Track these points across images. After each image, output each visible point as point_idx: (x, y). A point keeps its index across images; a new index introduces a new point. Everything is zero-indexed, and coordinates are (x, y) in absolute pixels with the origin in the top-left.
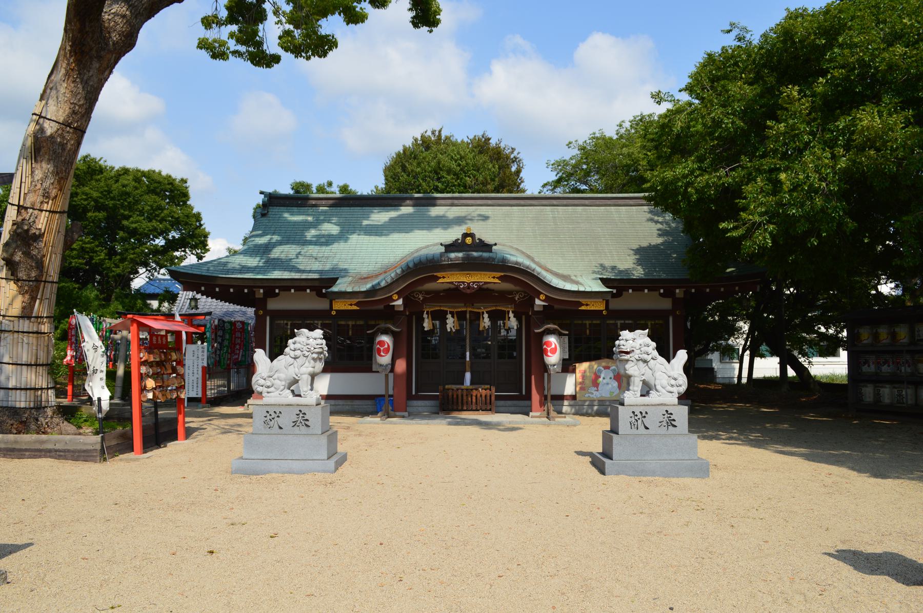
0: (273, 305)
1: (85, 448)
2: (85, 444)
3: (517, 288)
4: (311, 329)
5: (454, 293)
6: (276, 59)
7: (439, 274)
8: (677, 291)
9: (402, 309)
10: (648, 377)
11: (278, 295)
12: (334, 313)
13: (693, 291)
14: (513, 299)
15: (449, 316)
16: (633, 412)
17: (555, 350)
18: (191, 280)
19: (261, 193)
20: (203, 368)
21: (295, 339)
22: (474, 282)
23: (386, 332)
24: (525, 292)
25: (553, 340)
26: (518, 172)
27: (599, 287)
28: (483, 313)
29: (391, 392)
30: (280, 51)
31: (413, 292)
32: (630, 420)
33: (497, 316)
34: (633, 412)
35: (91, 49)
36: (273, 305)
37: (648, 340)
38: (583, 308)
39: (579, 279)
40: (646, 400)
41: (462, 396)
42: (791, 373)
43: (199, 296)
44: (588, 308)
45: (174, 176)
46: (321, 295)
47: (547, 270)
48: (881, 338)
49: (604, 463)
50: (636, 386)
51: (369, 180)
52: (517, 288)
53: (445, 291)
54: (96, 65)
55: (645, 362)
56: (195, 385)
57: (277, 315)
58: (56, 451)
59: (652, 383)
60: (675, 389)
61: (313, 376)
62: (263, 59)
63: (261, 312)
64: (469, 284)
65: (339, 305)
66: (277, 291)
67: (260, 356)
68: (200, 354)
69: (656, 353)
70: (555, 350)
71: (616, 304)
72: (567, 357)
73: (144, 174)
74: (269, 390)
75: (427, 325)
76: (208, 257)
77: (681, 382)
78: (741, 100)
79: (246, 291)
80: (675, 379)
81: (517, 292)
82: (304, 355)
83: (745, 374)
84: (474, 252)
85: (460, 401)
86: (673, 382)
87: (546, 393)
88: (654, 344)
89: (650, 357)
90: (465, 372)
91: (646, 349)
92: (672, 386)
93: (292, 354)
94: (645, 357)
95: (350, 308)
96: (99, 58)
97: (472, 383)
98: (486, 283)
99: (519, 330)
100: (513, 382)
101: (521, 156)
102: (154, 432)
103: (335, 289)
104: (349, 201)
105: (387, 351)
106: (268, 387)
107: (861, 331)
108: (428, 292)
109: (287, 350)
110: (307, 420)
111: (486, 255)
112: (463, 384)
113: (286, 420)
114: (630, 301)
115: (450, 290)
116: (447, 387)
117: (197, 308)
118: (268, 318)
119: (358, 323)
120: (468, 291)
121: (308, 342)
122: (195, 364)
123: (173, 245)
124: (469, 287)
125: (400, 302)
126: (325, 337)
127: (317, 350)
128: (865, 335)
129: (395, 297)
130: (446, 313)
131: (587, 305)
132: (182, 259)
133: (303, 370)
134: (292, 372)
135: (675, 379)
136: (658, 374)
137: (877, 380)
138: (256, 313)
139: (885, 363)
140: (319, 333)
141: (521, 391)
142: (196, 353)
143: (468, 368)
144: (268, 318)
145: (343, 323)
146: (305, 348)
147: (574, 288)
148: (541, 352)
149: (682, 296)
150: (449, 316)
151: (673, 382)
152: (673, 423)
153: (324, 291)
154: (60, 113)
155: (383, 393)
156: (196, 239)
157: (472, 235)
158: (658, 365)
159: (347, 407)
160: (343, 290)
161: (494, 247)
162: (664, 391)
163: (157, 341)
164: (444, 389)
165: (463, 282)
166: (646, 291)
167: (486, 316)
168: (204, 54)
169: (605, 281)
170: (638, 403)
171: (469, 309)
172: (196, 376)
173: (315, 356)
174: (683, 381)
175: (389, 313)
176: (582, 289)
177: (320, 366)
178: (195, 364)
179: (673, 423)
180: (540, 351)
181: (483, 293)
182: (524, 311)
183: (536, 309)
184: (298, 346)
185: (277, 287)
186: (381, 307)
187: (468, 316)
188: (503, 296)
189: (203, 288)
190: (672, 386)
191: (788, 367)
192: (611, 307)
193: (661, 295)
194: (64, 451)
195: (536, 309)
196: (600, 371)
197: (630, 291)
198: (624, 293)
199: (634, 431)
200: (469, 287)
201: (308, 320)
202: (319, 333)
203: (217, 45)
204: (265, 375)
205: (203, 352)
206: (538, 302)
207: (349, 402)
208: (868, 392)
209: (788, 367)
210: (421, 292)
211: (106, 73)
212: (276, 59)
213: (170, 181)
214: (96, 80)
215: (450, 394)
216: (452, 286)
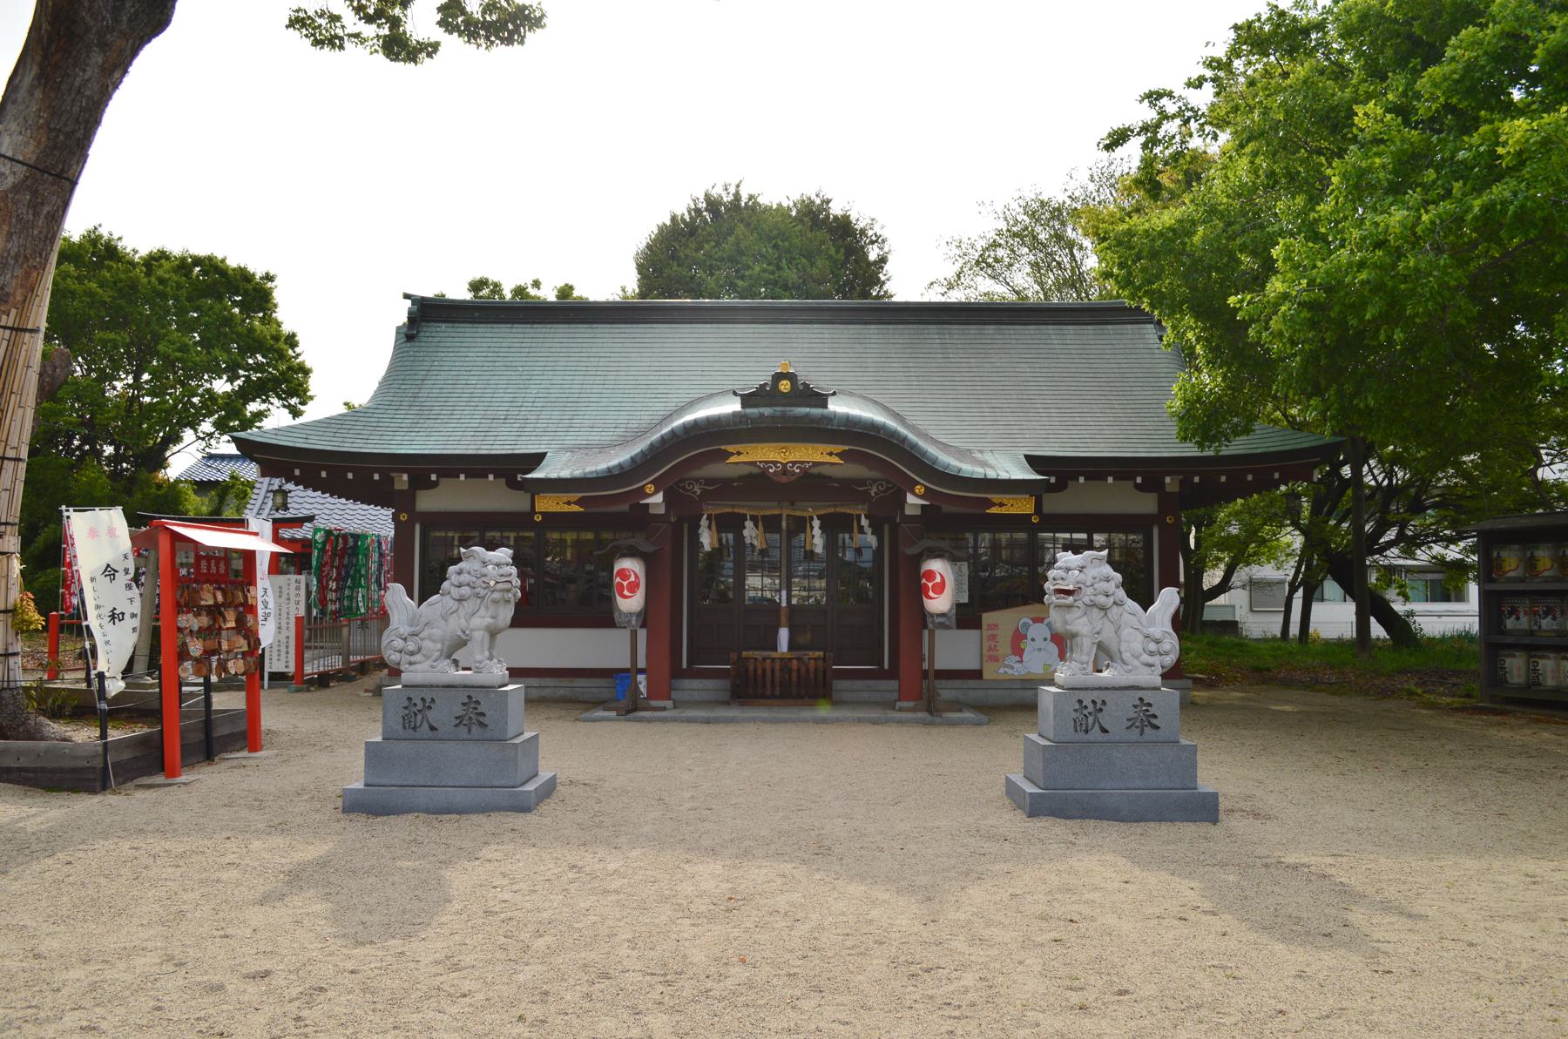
0: (427, 502)
1: (72, 764)
2: (76, 757)
3: (874, 474)
4: (491, 547)
5: (759, 483)
6: (432, 49)
7: (730, 448)
8: (1168, 480)
9: (662, 511)
10: (1108, 635)
11: (435, 484)
12: (538, 518)
13: (1197, 479)
14: (867, 492)
15: (749, 524)
16: (1080, 702)
18: (281, 461)
19: (407, 296)
20: (298, 620)
21: (461, 565)
22: (794, 463)
23: (632, 553)
24: (888, 482)
25: (937, 566)
26: (883, 260)
27: (1019, 472)
28: (811, 519)
29: (642, 664)
30: (437, 34)
31: (683, 481)
32: (1075, 715)
33: (835, 525)
34: (1080, 702)
35: (88, 30)
36: (427, 502)
38: (994, 510)
39: (988, 457)
41: (773, 670)
42: (1377, 630)
43: (290, 486)
44: (1003, 511)
45: (251, 269)
47: (926, 437)
48: (1540, 567)
50: (1084, 652)
51: (611, 278)
52: (874, 474)
53: (741, 478)
54: (97, 58)
55: (1103, 608)
56: (283, 649)
57: (433, 520)
58: (20, 770)
59: (1113, 647)
60: (1156, 660)
61: (493, 633)
62: (399, 47)
63: (403, 517)
64: (784, 465)
65: (549, 504)
66: (434, 477)
67: (397, 597)
68: (293, 592)
69: (1121, 593)
71: (1056, 504)
72: (965, 600)
73: (198, 261)
74: (413, 659)
75: (707, 539)
76: (313, 412)
77: (1166, 646)
78: (1378, 141)
79: (376, 477)
80: (1158, 642)
81: (874, 481)
82: (477, 595)
83: (1294, 629)
84: (785, 408)
86: (1152, 647)
87: (925, 666)
88: (1118, 577)
89: (1111, 600)
90: (778, 626)
91: (1104, 586)
92: (1151, 654)
93: (455, 592)
94: (1102, 599)
95: (566, 509)
96: (104, 46)
97: (791, 647)
98: (816, 464)
99: (878, 553)
101: (884, 233)
102: (202, 736)
103: (537, 474)
104: (570, 312)
105: (633, 587)
106: (412, 654)
107: (1504, 554)
108: (710, 481)
109: (445, 585)
110: (483, 714)
112: (775, 649)
113: (443, 714)
114: (1081, 498)
115: (750, 476)
116: (745, 654)
117: (287, 509)
120: (784, 479)
121: (484, 571)
122: (284, 610)
123: (247, 394)
124: (785, 472)
125: (658, 498)
126: (517, 561)
127: (500, 586)
128: (1511, 561)
129: (650, 489)
130: (744, 517)
132: (260, 415)
133: (477, 622)
134: (455, 625)
135: (1158, 642)
137: (1533, 647)
138: (395, 518)
139: (1546, 614)
140: (504, 554)
141: (881, 663)
142: (285, 591)
143: (783, 619)
146: (479, 582)
147: (978, 472)
148: (919, 592)
150: (749, 524)
151: (1152, 647)
152: (1153, 721)
153: (519, 477)
154: (31, 148)
155: (627, 665)
156: (290, 383)
157: (791, 377)
158: (1126, 615)
159: (562, 692)
160: (554, 475)
162: (1136, 663)
163: (209, 568)
164: (740, 658)
165: (775, 463)
166: (1110, 480)
167: (816, 523)
168: (298, 41)
169: (1033, 461)
170: (457, 682)
171: (785, 512)
172: (284, 633)
173: (496, 596)
174: (1171, 643)
175: (639, 518)
176: (991, 474)
177: (507, 613)
178: (284, 610)
179: (1153, 721)
180: (914, 587)
181: (811, 483)
182: (886, 515)
183: (908, 512)
184: (465, 578)
185: (298, 466)
186: (625, 507)
187: (784, 524)
188: (848, 489)
189: (297, 472)
190: (1151, 654)
191: (1372, 619)
193: (1137, 487)
194: (35, 770)
195: (908, 512)
196: (1027, 626)
197: (1082, 480)
198: (1071, 484)
199: (1081, 736)
200: (785, 472)
201: (484, 528)
202: (504, 554)
203: (323, 22)
204: (405, 630)
205: (298, 588)
207: (565, 682)
208: (1515, 667)
209: (1372, 619)
210: (697, 480)
211: (117, 75)
212: (432, 49)
213: (244, 275)
214: (96, 88)
215: (751, 667)
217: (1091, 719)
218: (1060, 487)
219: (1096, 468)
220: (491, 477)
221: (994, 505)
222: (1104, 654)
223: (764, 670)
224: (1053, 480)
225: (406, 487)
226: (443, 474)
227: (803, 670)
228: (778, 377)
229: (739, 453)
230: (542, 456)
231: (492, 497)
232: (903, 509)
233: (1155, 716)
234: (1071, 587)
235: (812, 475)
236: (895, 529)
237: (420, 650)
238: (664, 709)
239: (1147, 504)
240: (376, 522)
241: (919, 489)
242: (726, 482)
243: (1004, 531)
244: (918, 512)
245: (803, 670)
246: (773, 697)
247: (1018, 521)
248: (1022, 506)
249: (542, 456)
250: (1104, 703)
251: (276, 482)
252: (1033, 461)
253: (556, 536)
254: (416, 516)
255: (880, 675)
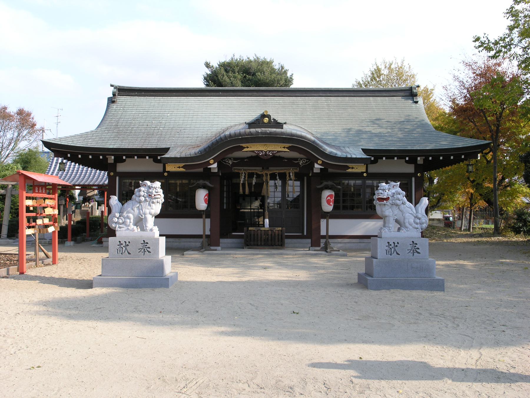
0: (121, 168)
3: (302, 156)
5: (255, 160)
7: (244, 145)
8: (419, 158)
9: (216, 171)
10: (399, 216)
11: (125, 161)
13: (430, 158)
16: (388, 243)
17: (327, 200)
19: (112, 86)
22: (270, 151)
27: (360, 155)
31: (224, 159)
34: (388, 243)
36: (121, 168)
37: (400, 190)
38: (350, 170)
40: (399, 234)
41: (261, 235)
46: (156, 161)
49: (366, 280)
53: (248, 158)
57: (124, 175)
59: (402, 221)
63: (112, 174)
64: (266, 152)
65: (171, 168)
66: (124, 158)
69: (405, 198)
70: (327, 200)
71: (374, 169)
81: (301, 159)
85: (259, 238)
98: (278, 152)
100: (297, 229)
103: (166, 156)
108: (235, 159)
109: (134, 196)
111: (278, 130)
118: (117, 178)
119: (184, 181)
124: (266, 155)
125: (215, 165)
129: (212, 162)
131: (353, 168)
136: (407, 215)
141: (303, 232)
144: (117, 178)
145: (173, 182)
149: (422, 162)
152: (418, 250)
153: (159, 158)
157: (269, 116)
160: (173, 156)
161: (284, 125)
162: (411, 227)
165: (262, 151)
181: (275, 160)
182: (304, 174)
183: (315, 171)
185: (124, 155)
186: (201, 170)
188: (291, 162)
189: (69, 155)
190: (417, 224)
192: (369, 171)
193: (407, 162)
195: (315, 171)
197: (384, 158)
198: (379, 160)
200: (266, 155)
206: (316, 166)
210: (230, 159)
216: (254, 154)
217: (393, 250)
218: (375, 162)
219: (390, 154)
220: (147, 157)
221: (350, 168)
222: (400, 224)
223: (258, 235)
224: (373, 159)
225: (113, 162)
226: (128, 156)
227: (273, 234)
228: (263, 116)
229: (247, 147)
230: (168, 149)
231: (147, 165)
232: (313, 170)
233: (418, 249)
234: (385, 197)
235: (277, 157)
236: (309, 179)
237: (123, 223)
238: (216, 250)
239: (410, 169)
240: (101, 177)
241: (319, 162)
242: (242, 159)
243: (352, 179)
244: (319, 171)
245: (273, 234)
246: (261, 245)
247: (359, 175)
248: (360, 168)
249: (168, 149)
250: (398, 243)
251: (60, 160)
252: (364, 150)
253: (173, 182)
254: (117, 174)
255: (302, 237)
